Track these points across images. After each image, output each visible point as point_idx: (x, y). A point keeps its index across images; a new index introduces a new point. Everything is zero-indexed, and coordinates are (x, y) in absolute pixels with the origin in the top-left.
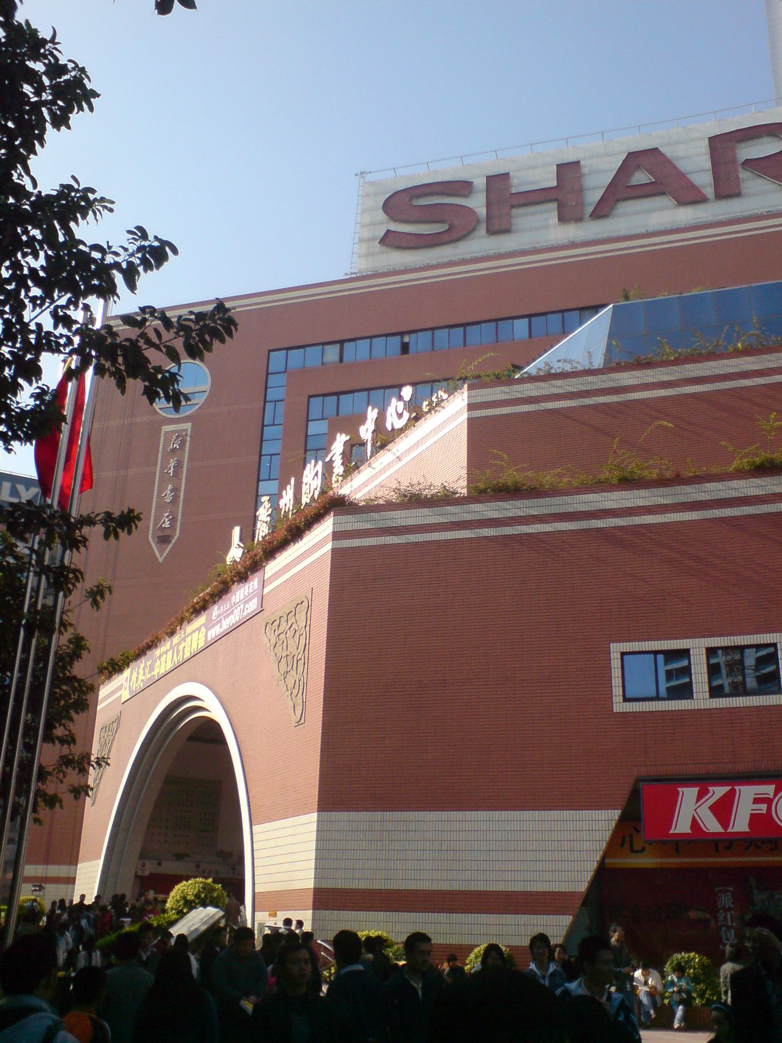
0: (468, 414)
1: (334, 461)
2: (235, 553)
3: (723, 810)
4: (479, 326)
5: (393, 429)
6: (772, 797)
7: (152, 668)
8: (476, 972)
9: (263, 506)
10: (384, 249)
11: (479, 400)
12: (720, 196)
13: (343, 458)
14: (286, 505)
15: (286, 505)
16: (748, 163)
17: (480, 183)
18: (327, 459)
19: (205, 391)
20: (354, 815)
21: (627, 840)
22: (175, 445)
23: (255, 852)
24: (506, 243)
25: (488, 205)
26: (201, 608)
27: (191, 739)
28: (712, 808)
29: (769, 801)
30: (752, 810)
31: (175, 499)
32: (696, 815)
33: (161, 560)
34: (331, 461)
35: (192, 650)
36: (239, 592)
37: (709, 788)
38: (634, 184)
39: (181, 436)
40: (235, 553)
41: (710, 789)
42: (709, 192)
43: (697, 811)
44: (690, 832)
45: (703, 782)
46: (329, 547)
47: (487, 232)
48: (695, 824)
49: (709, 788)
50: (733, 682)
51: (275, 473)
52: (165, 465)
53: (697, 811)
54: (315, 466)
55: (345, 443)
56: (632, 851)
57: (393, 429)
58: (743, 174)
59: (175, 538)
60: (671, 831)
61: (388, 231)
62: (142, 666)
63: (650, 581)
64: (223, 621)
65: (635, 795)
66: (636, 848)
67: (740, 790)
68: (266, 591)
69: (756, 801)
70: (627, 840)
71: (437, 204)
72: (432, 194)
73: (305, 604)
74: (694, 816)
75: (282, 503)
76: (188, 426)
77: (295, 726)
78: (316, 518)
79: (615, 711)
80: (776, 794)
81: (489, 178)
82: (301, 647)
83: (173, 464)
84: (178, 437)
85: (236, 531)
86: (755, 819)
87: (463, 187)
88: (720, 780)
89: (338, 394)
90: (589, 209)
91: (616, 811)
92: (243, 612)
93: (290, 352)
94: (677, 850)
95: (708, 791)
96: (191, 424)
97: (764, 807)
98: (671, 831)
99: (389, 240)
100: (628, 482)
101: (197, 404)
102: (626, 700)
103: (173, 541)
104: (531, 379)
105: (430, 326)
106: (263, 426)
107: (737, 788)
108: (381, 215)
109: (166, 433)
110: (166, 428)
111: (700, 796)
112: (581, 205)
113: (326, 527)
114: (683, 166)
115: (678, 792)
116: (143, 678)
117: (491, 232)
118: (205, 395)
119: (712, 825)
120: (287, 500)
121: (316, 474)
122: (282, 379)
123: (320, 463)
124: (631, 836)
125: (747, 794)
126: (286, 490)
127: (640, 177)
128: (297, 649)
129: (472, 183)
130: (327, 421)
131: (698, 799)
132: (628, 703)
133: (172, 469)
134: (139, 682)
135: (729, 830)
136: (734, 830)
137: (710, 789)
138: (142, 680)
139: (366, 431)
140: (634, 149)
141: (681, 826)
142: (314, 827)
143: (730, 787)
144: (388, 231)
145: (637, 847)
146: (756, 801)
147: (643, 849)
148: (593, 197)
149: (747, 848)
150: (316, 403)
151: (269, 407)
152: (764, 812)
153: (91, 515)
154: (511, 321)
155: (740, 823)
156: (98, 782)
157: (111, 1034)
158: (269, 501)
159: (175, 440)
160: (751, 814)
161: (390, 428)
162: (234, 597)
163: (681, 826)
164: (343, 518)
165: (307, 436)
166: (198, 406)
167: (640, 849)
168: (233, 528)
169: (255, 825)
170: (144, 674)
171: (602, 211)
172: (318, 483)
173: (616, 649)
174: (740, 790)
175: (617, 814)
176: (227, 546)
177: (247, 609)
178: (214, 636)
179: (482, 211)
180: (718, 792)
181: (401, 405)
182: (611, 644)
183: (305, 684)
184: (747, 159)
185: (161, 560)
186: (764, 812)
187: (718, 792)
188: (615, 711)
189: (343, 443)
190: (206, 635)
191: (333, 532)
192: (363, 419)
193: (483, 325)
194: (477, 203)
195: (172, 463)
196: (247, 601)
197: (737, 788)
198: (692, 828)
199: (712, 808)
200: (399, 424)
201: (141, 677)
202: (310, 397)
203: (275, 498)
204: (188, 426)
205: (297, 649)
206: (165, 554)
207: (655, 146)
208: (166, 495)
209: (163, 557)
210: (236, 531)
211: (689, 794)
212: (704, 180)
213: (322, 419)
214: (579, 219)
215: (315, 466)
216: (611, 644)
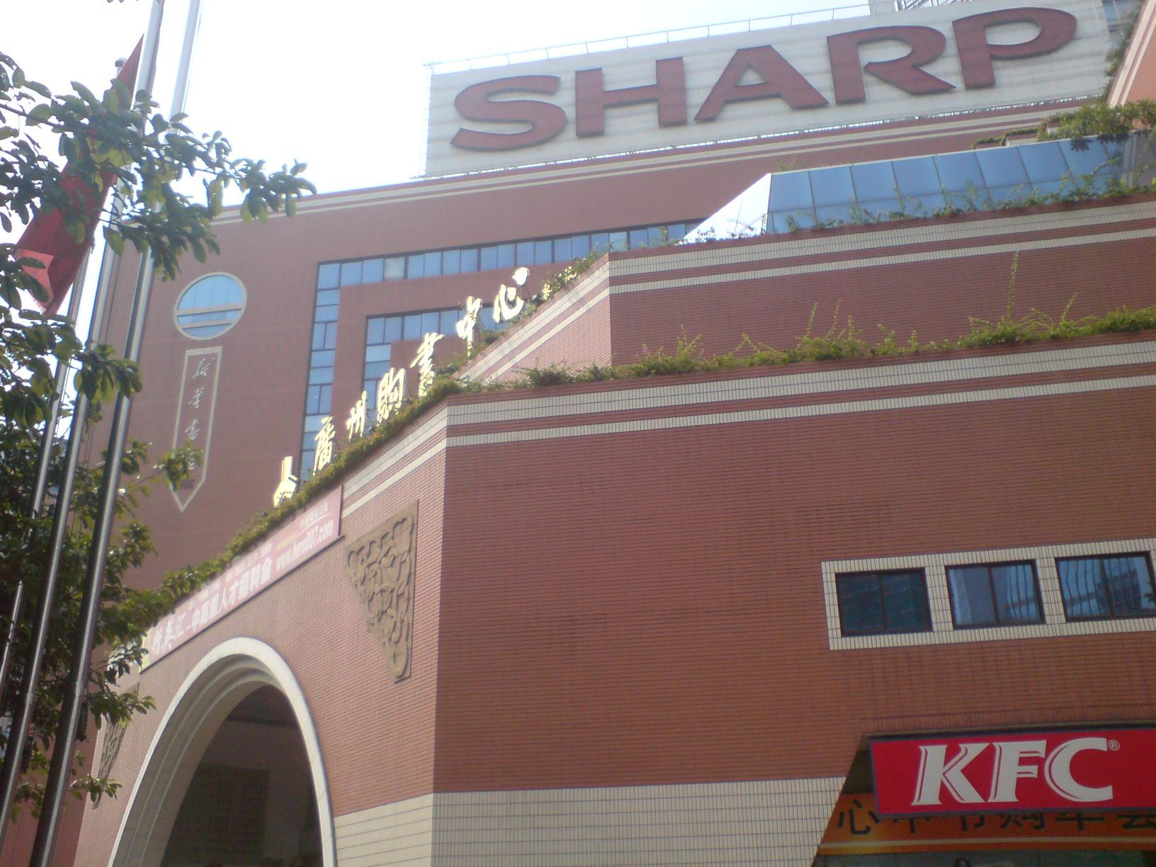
0: (448, 442)
1: (421, 366)
2: (286, 488)
3: (980, 773)
4: (570, 239)
5: (502, 321)
6: (1043, 755)
7: (188, 620)
9: (324, 428)
11: (623, 272)
12: (843, 101)
13: (433, 362)
14: (355, 425)
15: (355, 425)
16: (873, 68)
17: (568, 79)
18: (413, 365)
19: (241, 309)
20: (483, 796)
21: (846, 819)
22: (202, 372)
23: (338, 852)
24: (600, 149)
26: (246, 547)
27: (231, 718)
28: (967, 772)
29: (1039, 762)
30: (1019, 773)
31: (201, 436)
32: (945, 781)
33: (182, 508)
34: (418, 367)
35: (252, 586)
37: (961, 746)
38: (745, 84)
39: (210, 359)
40: (286, 488)
41: (962, 746)
42: (829, 96)
43: (946, 775)
44: (940, 803)
45: (952, 740)
46: (442, 445)
47: (577, 134)
48: (944, 793)
49: (961, 746)
51: (326, 406)
52: (189, 395)
53: (946, 775)
54: (395, 374)
55: (435, 343)
56: (853, 831)
57: (502, 321)
58: (868, 79)
59: (201, 483)
60: (915, 803)
61: (461, 131)
62: (170, 623)
63: (360, 751)
64: (295, 546)
65: (862, 759)
66: (858, 827)
67: (1000, 747)
68: (346, 513)
69: (1023, 761)
70: (846, 819)
71: (519, 101)
72: (512, 90)
73: (409, 523)
74: (942, 782)
75: (349, 423)
76: (218, 350)
77: (396, 683)
78: (428, 407)
79: (832, 649)
80: (1049, 750)
82: (404, 578)
83: (199, 395)
84: (205, 363)
85: (287, 463)
86: (1023, 785)
88: (974, 736)
89: (403, 315)
90: (693, 112)
91: (840, 779)
92: (318, 536)
93: (344, 265)
94: (913, 830)
95: (959, 750)
96: (221, 347)
97: (1033, 770)
98: (915, 803)
99: (464, 142)
100: (830, 360)
101: (230, 324)
102: (1032, 563)
103: (199, 486)
104: (689, 248)
105: (513, 238)
106: (311, 351)
107: (996, 745)
108: (451, 113)
109: (191, 358)
110: (190, 353)
111: (949, 757)
112: (683, 105)
113: (438, 422)
115: (920, 752)
116: (173, 637)
117: (583, 135)
118: (238, 315)
119: (967, 793)
120: (357, 418)
121: (397, 384)
122: (334, 297)
123: (402, 372)
124: (851, 812)
125: (1009, 755)
126: (355, 407)
127: (751, 78)
128: (398, 580)
129: (559, 78)
130: (390, 346)
131: (948, 759)
132: (848, 639)
133: (198, 401)
134: (166, 642)
135: (991, 800)
136: (997, 800)
137: (962, 746)
138: (171, 641)
139: (465, 329)
140: (742, 47)
141: (927, 795)
142: (429, 813)
143: (988, 744)
144: (461, 131)
145: (859, 826)
146: (1023, 761)
147: (868, 829)
148: (697, 100)
149: (1004, 826)
150: (375, 327)
151: (318, 329)
152: (1035, 775)
154: (607, 234)
155: (1005, 791)
156: (104, 775)
158: (331, 422)
159: (202, 366)
160: (1019, 780)
161: (497, 320)
162: (303, 521)
163: (927, 795)
164: (461, 409)
165: (364, 363)
166: (229, 328)
167: (864, 828)
168: (283, 459)
169: (337, 816)
170: (174, 632)
171: (708, 115)
172: (399, 394)
173: (830, 570)
174: (1000, 747)
175: (840, 782)
176: (275, 480)
177: (322, 534)
178: (283, 566)
180: (973, 750)
181: (512, 292)
182: (823, 563)
183: (411, 626)
184: (870, 63)
185: (182, 508)
186: (1035, 775)
187: (973, 750)
188: (832, 649)
189: (432, 345)
190: (274, 566)
191: (448, 426)
192: (460, 309)
193: (574, 238)
194: (565, 100)
195: (198, 394)
196: (321, 524)
197: (996, 745)
198: (940, 798)
199: (967, 772)
200: (509, 314)
201: (169, 637)
202: (368, 317)
203: (339, 419)
204: (218, 350)
205: (398, 580)
206: (188, 502)
207: (768, 44)
208: (190, 430)
209: (185, 505)
210: (287, 463)
211: (933, 754)
212: (822, 82)
213: (383, 344)
214: (680, 122)
215: (395, 374)
216: (823, 563)
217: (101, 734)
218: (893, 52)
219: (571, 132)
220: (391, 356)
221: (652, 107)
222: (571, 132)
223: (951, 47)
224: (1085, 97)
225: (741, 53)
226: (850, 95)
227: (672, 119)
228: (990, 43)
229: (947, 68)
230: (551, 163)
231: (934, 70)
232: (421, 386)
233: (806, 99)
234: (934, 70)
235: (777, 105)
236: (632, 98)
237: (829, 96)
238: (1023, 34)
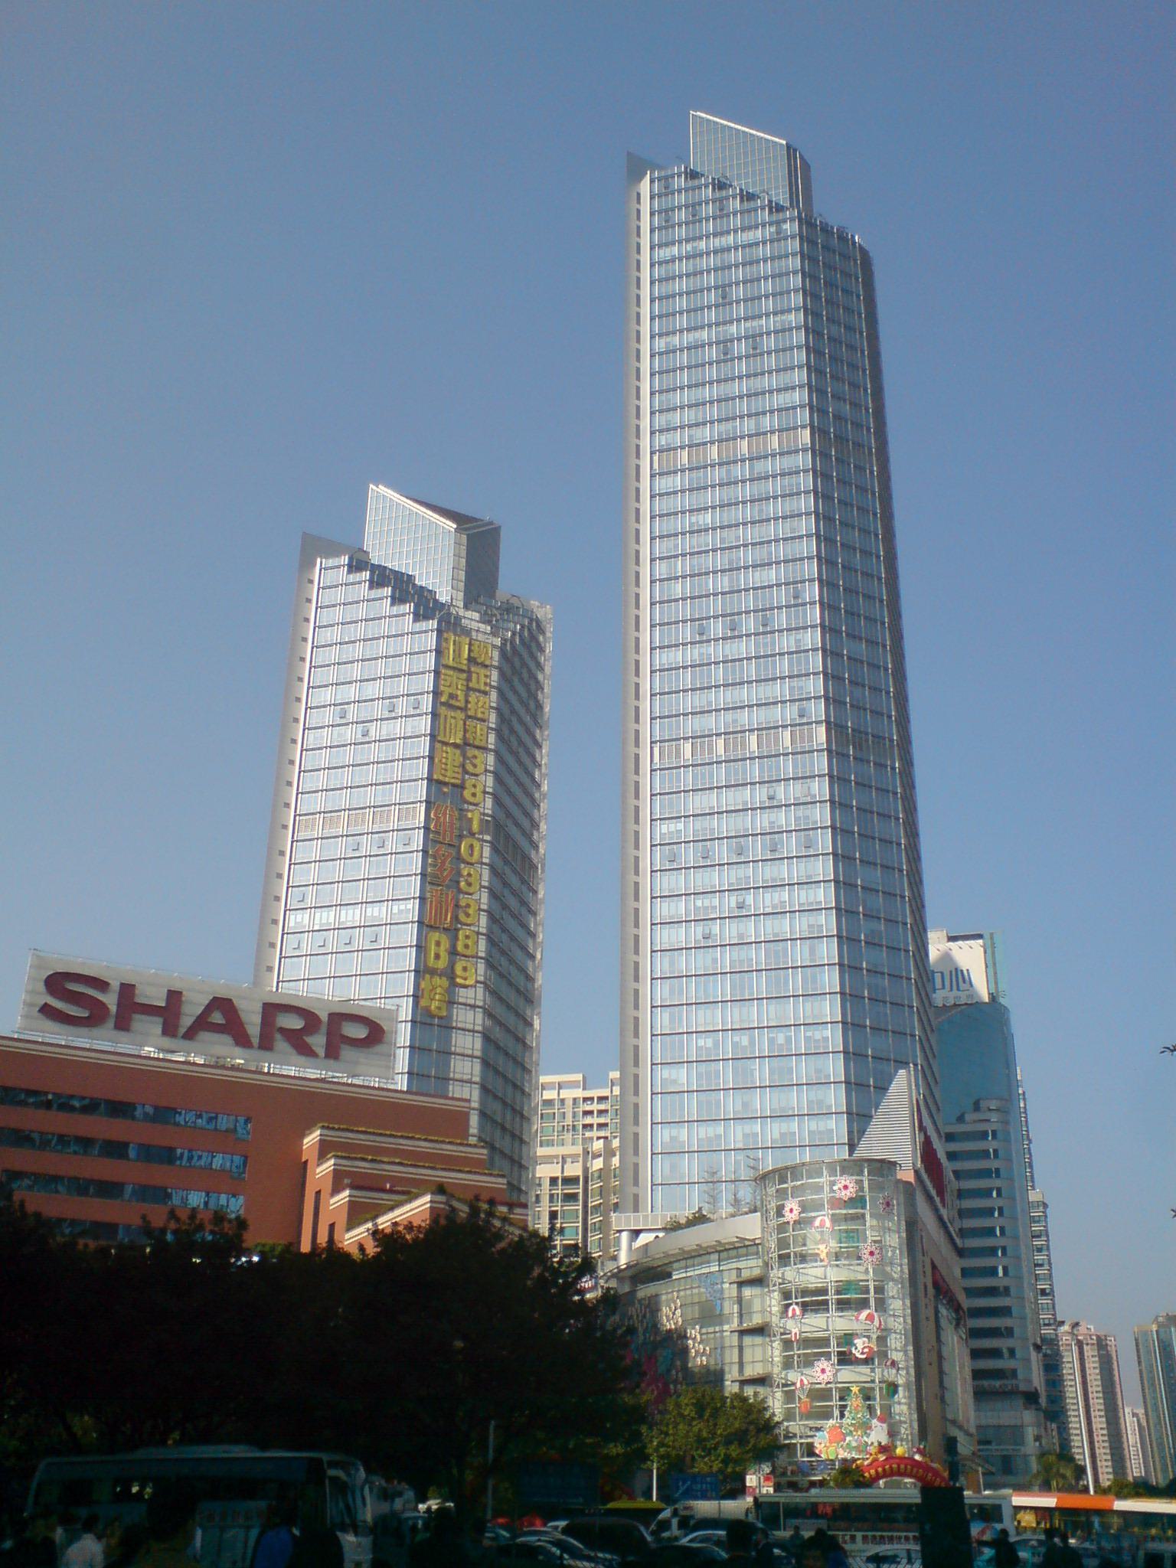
8: (44, 1225)
10: (41, 1016)
16: (282, 1030)
17: (115, 985)
25: (119, 1005)
36: (959, 1445)
42: (255, 1041)
50: (1040, 1486)
58: (278, 1036)
81: (122, 984)
87: (101, 985)
90: (182, 1031)
99: (46, 1010)
108: (41, 987)
112: (176, 1027)
114: (244, 1017)
127: (217, 1018)
153: (82, 1151)
157: (581, 1542)
171: (190, 1035)
179: (113, 1009)
194: (110, 1000)
217: (537, 773)
218: (296, 1023)
219: (111, 1023)
220: (577, 1073)
221: (160, 1020)
222: (111, 1023)
223: (324, 1029)
224: (1019, 1078)
225: (215, 999)
226: (266, 1044)
227: (169, 1030)
228: (346, 1034)
229: (318, 1041)
230: (238, 1061)
231: (310, 1040)
232: (390, 1216)
233: (242, 1039)
234: (310, 1040)
235: (227, 1039)
236: (150, 1010)
237: (255, 1041)
238: (360, 1032)
